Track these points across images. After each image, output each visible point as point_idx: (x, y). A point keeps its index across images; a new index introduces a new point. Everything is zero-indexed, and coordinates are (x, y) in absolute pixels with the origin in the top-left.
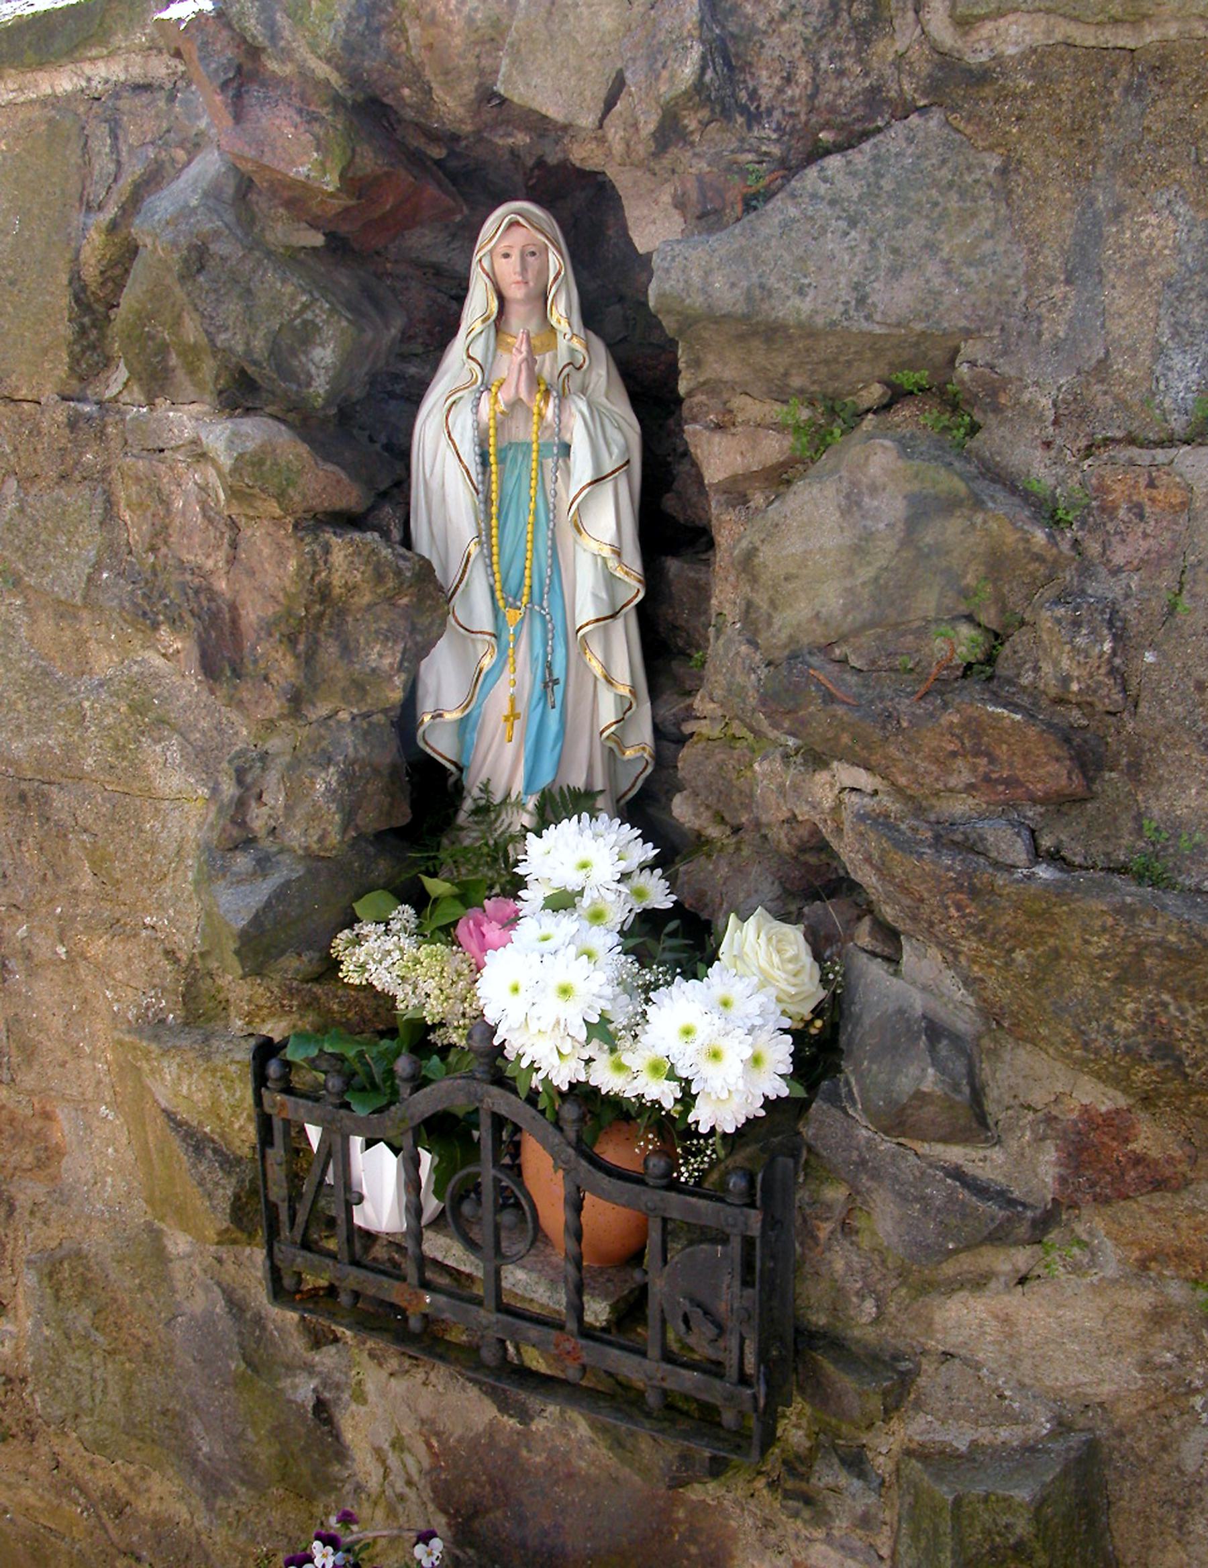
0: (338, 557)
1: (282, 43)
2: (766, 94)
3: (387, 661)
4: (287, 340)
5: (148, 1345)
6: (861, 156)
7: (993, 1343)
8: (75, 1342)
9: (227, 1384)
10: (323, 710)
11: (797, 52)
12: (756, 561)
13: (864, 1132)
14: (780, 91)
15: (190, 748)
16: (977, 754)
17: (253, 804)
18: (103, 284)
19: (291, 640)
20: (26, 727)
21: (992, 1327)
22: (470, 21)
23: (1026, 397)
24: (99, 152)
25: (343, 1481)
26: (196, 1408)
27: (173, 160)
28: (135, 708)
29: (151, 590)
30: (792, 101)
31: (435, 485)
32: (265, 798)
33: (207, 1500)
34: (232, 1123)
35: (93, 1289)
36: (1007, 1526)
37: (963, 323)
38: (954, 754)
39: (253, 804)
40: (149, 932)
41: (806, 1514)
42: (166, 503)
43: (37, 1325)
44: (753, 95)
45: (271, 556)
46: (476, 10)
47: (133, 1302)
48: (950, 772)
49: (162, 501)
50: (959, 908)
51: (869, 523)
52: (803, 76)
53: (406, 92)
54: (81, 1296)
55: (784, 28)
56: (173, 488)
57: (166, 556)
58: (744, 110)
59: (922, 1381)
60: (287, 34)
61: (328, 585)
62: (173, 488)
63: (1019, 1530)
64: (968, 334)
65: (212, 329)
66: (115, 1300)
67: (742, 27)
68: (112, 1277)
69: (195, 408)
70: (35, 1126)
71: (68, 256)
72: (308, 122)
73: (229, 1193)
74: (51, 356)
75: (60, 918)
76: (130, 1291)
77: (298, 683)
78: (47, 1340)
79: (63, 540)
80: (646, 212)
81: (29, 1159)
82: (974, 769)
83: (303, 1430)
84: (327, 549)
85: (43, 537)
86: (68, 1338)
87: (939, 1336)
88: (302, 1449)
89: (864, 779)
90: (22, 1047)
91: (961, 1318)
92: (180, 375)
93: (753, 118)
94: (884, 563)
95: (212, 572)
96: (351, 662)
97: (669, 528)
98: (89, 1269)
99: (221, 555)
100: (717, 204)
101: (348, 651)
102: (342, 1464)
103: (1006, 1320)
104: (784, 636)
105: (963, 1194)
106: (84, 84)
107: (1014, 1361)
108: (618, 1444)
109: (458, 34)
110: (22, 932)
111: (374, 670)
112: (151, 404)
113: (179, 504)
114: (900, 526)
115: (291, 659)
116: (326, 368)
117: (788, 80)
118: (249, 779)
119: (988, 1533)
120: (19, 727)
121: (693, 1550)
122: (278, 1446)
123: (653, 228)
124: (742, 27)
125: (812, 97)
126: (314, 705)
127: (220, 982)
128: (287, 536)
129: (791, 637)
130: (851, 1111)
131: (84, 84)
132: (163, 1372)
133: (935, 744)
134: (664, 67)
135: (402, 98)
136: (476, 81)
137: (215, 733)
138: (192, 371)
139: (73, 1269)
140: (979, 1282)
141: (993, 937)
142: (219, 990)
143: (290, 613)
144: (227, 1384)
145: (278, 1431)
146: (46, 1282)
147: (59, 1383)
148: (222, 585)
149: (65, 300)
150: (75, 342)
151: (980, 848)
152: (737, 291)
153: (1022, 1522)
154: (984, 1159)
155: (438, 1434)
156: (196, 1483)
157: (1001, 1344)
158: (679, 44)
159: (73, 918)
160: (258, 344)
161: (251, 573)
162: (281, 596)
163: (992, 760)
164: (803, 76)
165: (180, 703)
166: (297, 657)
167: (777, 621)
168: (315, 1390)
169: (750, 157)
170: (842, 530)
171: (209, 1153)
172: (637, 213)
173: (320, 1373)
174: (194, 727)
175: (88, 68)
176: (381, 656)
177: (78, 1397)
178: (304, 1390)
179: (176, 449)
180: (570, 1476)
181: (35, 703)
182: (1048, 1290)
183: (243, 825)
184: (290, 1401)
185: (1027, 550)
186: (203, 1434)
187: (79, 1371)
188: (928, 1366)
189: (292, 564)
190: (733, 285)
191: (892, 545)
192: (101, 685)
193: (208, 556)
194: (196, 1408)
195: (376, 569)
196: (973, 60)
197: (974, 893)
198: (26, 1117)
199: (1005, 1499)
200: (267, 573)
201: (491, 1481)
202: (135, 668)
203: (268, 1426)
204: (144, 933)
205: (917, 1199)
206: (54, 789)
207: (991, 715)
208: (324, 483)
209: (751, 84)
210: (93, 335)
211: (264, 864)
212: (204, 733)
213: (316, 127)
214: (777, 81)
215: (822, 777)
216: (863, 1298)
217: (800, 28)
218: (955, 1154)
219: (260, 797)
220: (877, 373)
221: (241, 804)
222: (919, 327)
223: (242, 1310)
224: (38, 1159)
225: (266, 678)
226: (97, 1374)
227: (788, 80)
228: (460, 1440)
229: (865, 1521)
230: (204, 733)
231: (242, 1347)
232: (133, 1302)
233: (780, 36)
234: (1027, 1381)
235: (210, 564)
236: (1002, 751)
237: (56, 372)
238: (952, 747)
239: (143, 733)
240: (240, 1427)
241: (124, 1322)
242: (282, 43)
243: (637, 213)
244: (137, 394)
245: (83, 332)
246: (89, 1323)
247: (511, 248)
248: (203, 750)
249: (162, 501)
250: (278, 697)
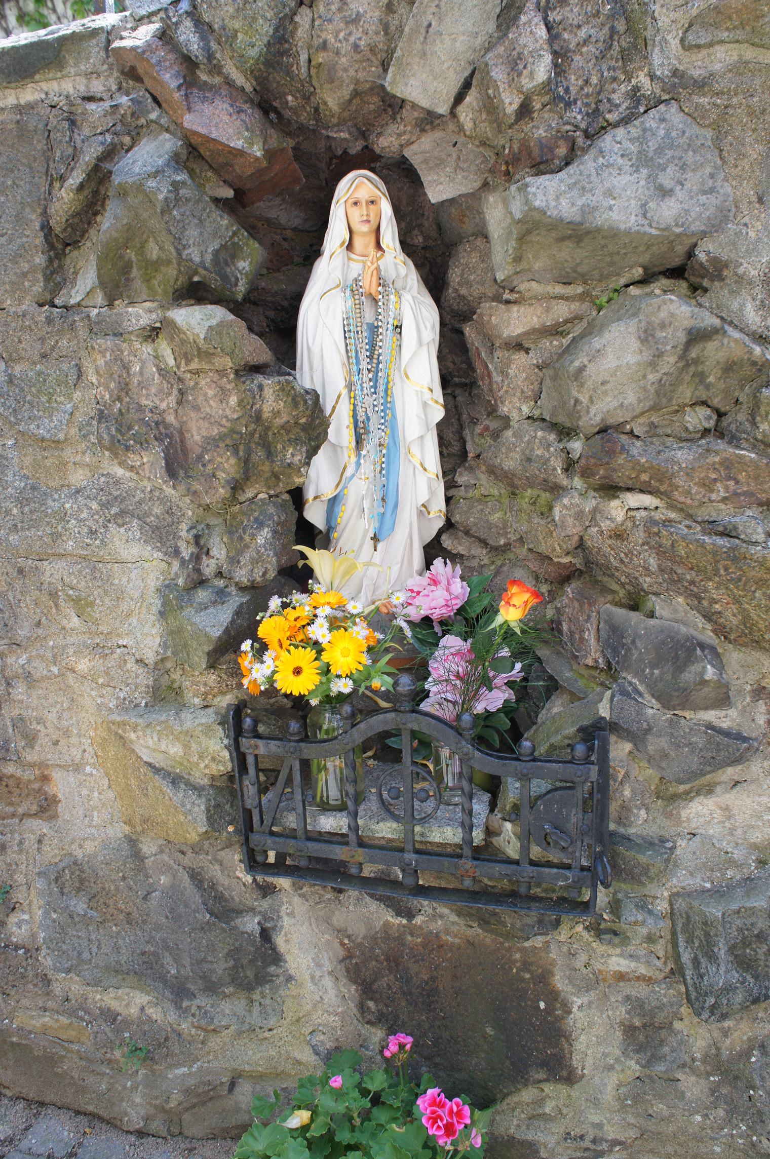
0: (269, 393)
1: (215, 62)
2: (573, 90)
3: (297, 458)
4: (223, 255)
5: (129, 914)
6: (634, 130)
7: (719, 823)
8: (77, 919)
9: (194, 929)
10: (250, 494)
11: (591, 65)
12: (585, 373)
13: (650, 711)
14: (582, 89)
15: (147, 528)
16: (729, 478)
17: (204, 558)
18: (65, 229)
19: (235, 449)
20: (19, 525)
21: (718, 814)
22: (356, 47)
23: (741, 270)
24: (61, 141)
25: (278, 976)
26: (167, 948)
27: (122, 144)
28: (105, 505)
29: (121, 425)
30: (587, 95)
31: (316, 350)
32: (211, 553)
33: (176, 1003)
34: (198, 764)
35: (87, 884)
36: (752, 924)
37: (703, 228)
38: (715, 480)
39: (204, 558)
40: (122, 649)
41: (616, 940)
42: (126, 367)
43: (47, 913)
44: (567, 90)
45: (215, 396)
46: (360, 39)
47: (117, 889)
48: (712, 491)
49: (125, 367)
50: (726, 569)
51: (660, 347)
52: (594, 80)
53: (290, 98)
54: (79, 890)
55: (584, 49)
56: (132, 358)
57: (128, 403)
58: (561, 99)
59: (678, 851)
60: (218, 55)
61: (259, 413)
62: (132, 358)
63: (760, 925)
64: (704, 234)
65: (180, 247)
66: (104, 889)
67: (562, 47)
68: (101, 874)
69: (148, 304)
70: (36, 786)
71: (39, 211)
72: (238, 112)
73: (203, 807)
74: (30, 277)
75: (53, 648)
76: (113, 881)
77: (238, 476)
78: (54, 921)
79: (44, 399)
80: (435, 178)
81: (35, 808)
82: (727, 489)
83: (252, 949)
84: (261, 387)
85: (28, 398)
86: (71, 917)
87: (685, 824)
88: (250, 961)
89: (647, 500)
90: (25, 736)
91: (700, 812)
92: (138, 284)
93: (568, 104)
94: (666, 370)
95: (164, 411)
96: (273, 461)
97: (460, 372)
98: (83, 872)
99: (172, 400)
100: (549, 157)
101: (270, 454)
102: (277, 965)
103: (727, 809)
104: (598, 419)
105: (719, 738)
106: (43, 96)
107: (731, 832)
108: (484, 922)
109: (344, 56)
110: (22, 661)
111: (289, 465)
112: (110, 305)
113: (136, 368)
114: (681, 347)
115: (233, 461)
116: (246, 274)
117: (587, 82)
118: (202, 543)
119: (740, 930)
120: (15, 526)
121: (527, 976)
122: (232, 962)
123: (441, 187)
124: (562, 47)
125: (599, 93)
126: (244, 491)
127: (173, 676)
128: (229, 382)
129: (602, 420)
130: (640, 700)
131: (43, 96)
132: (141, 928)
133: (703, 475)
134: (525, 67)
135: (287, 102)
136: (352, 87)
137: (167, 516)
138: (147, 280)
139: (72, 873)
140: (709, 790)
141: (745, 584)
142: (173, 681)
143: (233, 431)
144: (194, 929)
145: (234, 953)
146: (53, 885)
147: (64, 947)
148: (171, 418)
149: (39, 240)
150: (47, 267)
151: (734, 534)
152: (574, 209)
153: (761, 920)
154: (726, 716)
155: (349, 937)
156: (167, 993)
157: (723, 822)
158: (536, 54)
159: (64, 647)
160: (209, 258)
161: (197, 408)
162: (224, 421)
163: (737, 482)
164: (594, 80)
165: (137, 499)
166: (239, 459)
167: (593, 411)
168: (259, 923)
169: (568, 127)
170: (641, 352)
171: (182, 786)
172: (429, 178)
173: (260, 912)
174: (147, 514)
175: (44, 86)
176: (293, 455)
177: (80, 954)
178: (251, 924)
179: (131, 333)
180: (440, 946)
181: (27, 509)
182: (753, 787)
183: (198, 571)
184: (243, 933)
185: (749, 359)
186: (171, 962)
187: (79, 937)
188: (682, 843)
189: (233, 400)
190: (573, 204)
191: (672, 360)
192: (78, 492)
193: (162, 400)
194: (167, 948)
195: (293, 399)
196: (696, 73)
197: (735, 560)
198: (29, 781)
199: (750, 909)
200: (215, 407)
201: (388, 959)
202: (103, 479)
203: (226, 951)
204: (118, 651)
205: (686, 745)
206: (46, 563)
207: (737, 456)
208: (256, 349)
209: (565, 84)
210: (56, 264)
211: (221, 595)
212: (157, 517)
213: (243, 116)
214: (580, 83)
215: (615, 503)
216: (640, 809)
217: (593, 50)
218: (710, 716)
219: (208, 553)
220: (641, 260)
221: (197, 558)
222: (678, 230)
223: (201, 882)
224: (41, 807)
225: (214, 476)
226: (93, 937)
227: (587, 82)
228: (364, 938)
229: (650, 939)
230: (157, 517)
231: (205, 904)
232: (117, 889)
233: (581, 54)
234: (740, 841)
235: (163, 406)
236: (742, 476)
237: (34, 289)
238: (714, 476)
239: (109, 521)
240: (203, 954)
241: (111, 902)
242: (215, 62)
243: (429, 178)
244: (99, 298)
245: (51, 260)
246: (85, 906)
247: (358, 199)
248: (158, 528)
249: (125, 367)
250: (223, 487)
